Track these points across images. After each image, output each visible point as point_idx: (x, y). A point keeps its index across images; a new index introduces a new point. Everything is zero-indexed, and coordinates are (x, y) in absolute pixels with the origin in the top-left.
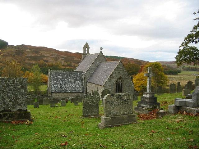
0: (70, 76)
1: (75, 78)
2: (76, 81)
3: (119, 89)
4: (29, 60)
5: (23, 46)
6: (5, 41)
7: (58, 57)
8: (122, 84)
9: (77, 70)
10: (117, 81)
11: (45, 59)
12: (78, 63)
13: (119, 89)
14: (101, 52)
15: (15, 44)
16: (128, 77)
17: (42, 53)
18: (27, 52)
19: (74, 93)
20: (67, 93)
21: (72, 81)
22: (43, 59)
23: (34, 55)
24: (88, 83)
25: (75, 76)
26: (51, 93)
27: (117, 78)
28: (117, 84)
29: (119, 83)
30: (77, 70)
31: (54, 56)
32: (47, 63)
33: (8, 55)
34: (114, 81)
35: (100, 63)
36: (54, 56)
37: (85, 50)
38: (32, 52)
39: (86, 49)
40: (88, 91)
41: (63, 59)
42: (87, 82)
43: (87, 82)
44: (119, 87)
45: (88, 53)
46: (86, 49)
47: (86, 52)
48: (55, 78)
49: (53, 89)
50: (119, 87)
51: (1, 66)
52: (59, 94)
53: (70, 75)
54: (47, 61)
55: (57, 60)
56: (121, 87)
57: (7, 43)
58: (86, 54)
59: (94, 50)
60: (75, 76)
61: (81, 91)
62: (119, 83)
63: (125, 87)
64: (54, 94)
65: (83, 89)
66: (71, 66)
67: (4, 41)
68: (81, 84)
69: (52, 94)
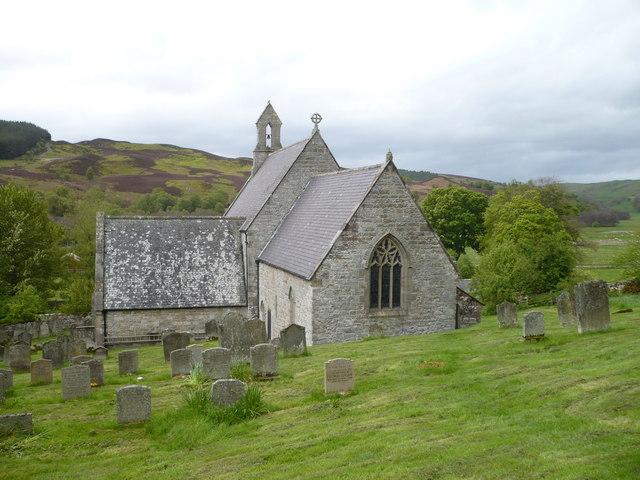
1: (210, 243)
2: (212, 261)
4: (117, 188)
5: (99, 143)
6: (39, 128)
7: (214, 177)
8: (398, 268)
10: (374, 257)
11: (170, 184)
12: (239, 183)
14: (317, 133)
15: (73, 138)
16: (428, 235)
17: (161, 165)
18: (112, 162)
19: (203, 308)
20: (175, 309)
21: (199, 258)
22: (164, 186)
23: (135, 172)
24: (261, 265)
25: (210, 238)
27: (374, 242)
28: (374, 270)
29: (387, 267)
30: (233, 212)
33: (49, 174)
34: (359, 256)
36: (199, 175)
37: (262, 134)
38: (129, 162)
39: (269, 130)
40: (262, 298)
41: (230, 182)
42: (258, 262)
43: (258, 262)
44: (386, 281)
45: (277, 145)
46: (269, 130)
47: (269, 143)
48: (125, 249)
52: (138, 316)
55: (210, 187)
56: (397, 281)
57: (47, 136)
58: (269, 151)
59: (295, 130)
60: (210, 238)
61: (236, 301)
62: (387, 267)
64: (118, 318)
65: (245, 289)
68: (234, 268)
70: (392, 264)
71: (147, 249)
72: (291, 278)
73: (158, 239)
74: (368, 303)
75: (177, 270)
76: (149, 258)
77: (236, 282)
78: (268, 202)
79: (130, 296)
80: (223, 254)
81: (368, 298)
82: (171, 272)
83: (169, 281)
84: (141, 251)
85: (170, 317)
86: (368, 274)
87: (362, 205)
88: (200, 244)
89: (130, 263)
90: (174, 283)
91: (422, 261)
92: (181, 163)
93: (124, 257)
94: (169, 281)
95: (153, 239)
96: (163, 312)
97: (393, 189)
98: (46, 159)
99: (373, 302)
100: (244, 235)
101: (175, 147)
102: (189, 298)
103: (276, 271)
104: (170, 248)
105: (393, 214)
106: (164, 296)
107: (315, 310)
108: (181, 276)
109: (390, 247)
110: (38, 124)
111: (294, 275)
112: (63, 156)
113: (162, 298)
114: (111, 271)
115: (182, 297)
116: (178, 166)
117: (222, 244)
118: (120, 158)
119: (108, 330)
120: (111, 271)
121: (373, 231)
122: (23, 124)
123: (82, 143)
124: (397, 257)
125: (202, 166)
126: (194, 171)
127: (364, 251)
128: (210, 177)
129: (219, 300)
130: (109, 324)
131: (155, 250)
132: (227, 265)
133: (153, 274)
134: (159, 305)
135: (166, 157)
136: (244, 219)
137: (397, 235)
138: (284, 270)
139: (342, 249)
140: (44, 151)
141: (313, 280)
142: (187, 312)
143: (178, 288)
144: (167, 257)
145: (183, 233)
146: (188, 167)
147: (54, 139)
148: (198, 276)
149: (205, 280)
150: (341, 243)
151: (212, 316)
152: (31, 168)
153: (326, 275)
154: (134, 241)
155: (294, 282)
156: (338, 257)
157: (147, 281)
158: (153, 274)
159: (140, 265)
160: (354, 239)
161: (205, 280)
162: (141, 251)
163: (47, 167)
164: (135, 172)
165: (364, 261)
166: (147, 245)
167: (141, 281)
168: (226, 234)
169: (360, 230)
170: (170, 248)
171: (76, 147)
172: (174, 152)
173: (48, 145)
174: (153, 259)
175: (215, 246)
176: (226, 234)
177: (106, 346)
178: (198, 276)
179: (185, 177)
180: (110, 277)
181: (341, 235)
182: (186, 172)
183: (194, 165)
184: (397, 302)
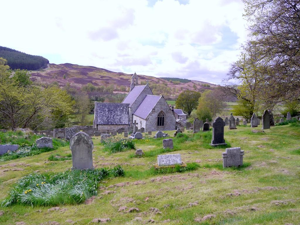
0: (116, 108)
1: (121, 110)
3: (161, 122)
5: (68, 65)
8: (163, 118)
9: (125, 102)
10: (159, 115)
13: (161, 122)
15: (57, 63)
17: (91, 74)
21: (119, 113)
23: (81, 77)
24: (134, 116)
25: (121, 108)
26: (97, 125)
27: (158, 112)
28: (158, 118)
29: (161, 118)
30: (125, 102)
31: (104, 78)
32: (97, 87)
34: (155, 115)
35: (146, 96)
36: (104, 78)
38: (79, 73)
41: (115, 82)
44: (161, 120)
49: (99, 121)
50: (161, 120)
51: (191, 224)
53: (116, 107)
54: (96, 84)
57: (48, 62)
60: (121, 108)
62: (161, 118)
63: (167, 121)
66: (125, 91)
67: (45, 58)
69: (98, 126)
70: (162, 117)
71: (107, 111)
72: (141, 119)
73: (109, 108)
74: (157, 125)
75: (114, 116)
76: (107, 113)
77: (127, 119)
78: (136, 101)
79: (103, 121)
80: (124, 112)
81: (157, 124)
82: (113, 116)
83: (112, 118)
84: (105, 111)
85: (112, 126)
86: (157, 118)
87: (157, 105)
88: (119, 110)
89: (103, 114)
90: (113, 119)
91: (169, 116)
92: (97, 74)
93: (101, 112)
94: (112, 118)
95: (108, 108)
96: (111, 125)
97: (163, 102)
98: (48, 70)
99: (158, 125)
100: (129, 108)
101: (95, 67)
102: (117, 123)
103: (137, 117)
104: (112, 110)
105: (163, 107)
106: (111, 122)
107: (146, 126)
108: (115, 117)
109: (162, 113)
110: (44, 57)
111: (142, 118)
112: (54, 69)
113: (110, 122)
114: (99, 116)
115: (115, 122)
116: (97, 75)
117: (124, 110)
118: (75, 71)
119: (98, 129)
120: (99, 116)
121: (158, 110)
122: (39, 57)
123: (61, 65)
124: (163, 115)
125: (105, 75)
126: (102, 77)
127: (156, 114)
128: (109, 79)
129: (124, 123)
130: (98, 128)
131: (109, 111)
132: (125, 115)
133: (108, 117)
134: (110, 124)
135: (92, 71)
136: (129, 104)
137: (163, 111)
138: (140, 117)
139: (152, 113)
140: (47, 67)
141: (146, 120)
142: (116, 126)
143: (114, 120)
144: (111, 113)
145: (115, 107)
146: (100, 75)
147: (50, 63)
148: (119, 117)
149: (120, 118)
150: (152, 112)
151: (122, 127)
152: (43, 73)
153: (148, 119)
154: (104, 109)
155: (142, 120)
156: (151, 115)
157: (107, 118)
158: (108, 117)
159: (105, 114)
160: (154, 112)
161: (120, 118)
162: (105, 111)
163: (49, 74)
164: (81, 77)
165: (156, 116)
166: (107, 110)
167: (106, 118)
168: (125, 108)
169: (156, 110)
170: (112, 110)
171: (58, 66)
172: (94, 69)
173: (48, 65)
174: (108, 113)
175: (123, 110)
176: (125, 108)
177: (224, 115)
178: (119, 117)
179: (99, 79)
180: (98, 117)
181: (152, 111)
182: (99, 77)
183: (102, 75)
184: (163, 125)
